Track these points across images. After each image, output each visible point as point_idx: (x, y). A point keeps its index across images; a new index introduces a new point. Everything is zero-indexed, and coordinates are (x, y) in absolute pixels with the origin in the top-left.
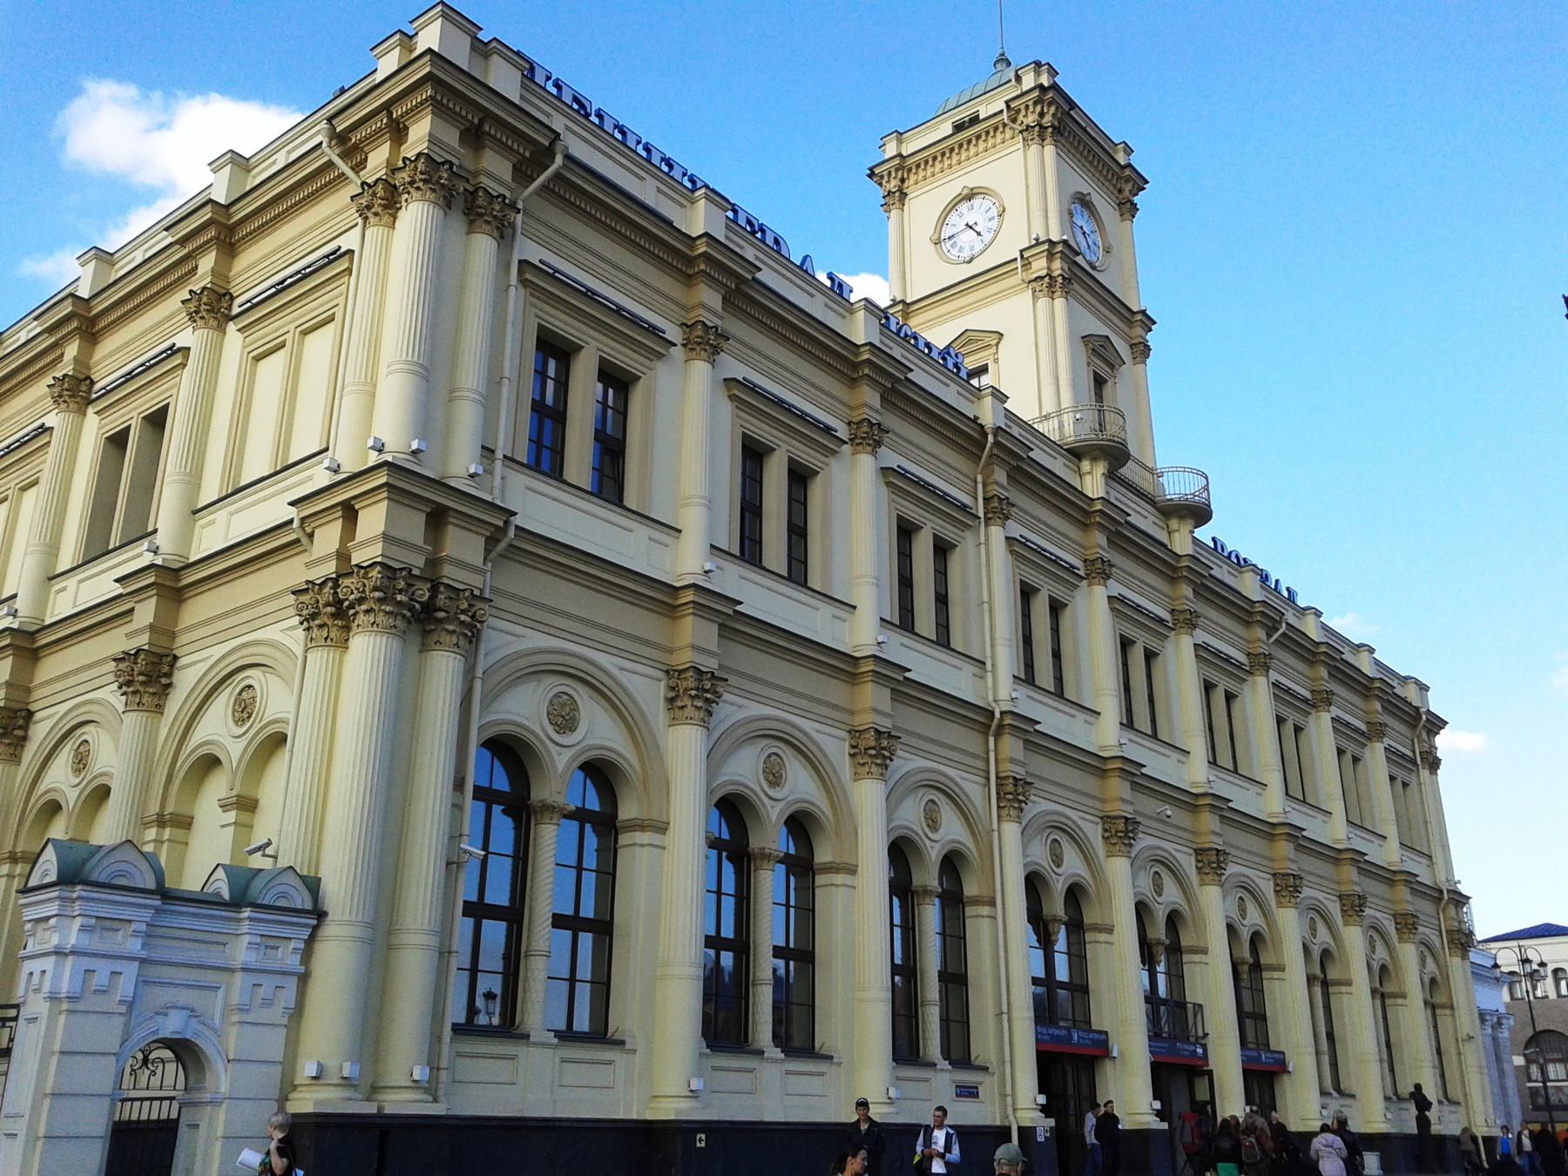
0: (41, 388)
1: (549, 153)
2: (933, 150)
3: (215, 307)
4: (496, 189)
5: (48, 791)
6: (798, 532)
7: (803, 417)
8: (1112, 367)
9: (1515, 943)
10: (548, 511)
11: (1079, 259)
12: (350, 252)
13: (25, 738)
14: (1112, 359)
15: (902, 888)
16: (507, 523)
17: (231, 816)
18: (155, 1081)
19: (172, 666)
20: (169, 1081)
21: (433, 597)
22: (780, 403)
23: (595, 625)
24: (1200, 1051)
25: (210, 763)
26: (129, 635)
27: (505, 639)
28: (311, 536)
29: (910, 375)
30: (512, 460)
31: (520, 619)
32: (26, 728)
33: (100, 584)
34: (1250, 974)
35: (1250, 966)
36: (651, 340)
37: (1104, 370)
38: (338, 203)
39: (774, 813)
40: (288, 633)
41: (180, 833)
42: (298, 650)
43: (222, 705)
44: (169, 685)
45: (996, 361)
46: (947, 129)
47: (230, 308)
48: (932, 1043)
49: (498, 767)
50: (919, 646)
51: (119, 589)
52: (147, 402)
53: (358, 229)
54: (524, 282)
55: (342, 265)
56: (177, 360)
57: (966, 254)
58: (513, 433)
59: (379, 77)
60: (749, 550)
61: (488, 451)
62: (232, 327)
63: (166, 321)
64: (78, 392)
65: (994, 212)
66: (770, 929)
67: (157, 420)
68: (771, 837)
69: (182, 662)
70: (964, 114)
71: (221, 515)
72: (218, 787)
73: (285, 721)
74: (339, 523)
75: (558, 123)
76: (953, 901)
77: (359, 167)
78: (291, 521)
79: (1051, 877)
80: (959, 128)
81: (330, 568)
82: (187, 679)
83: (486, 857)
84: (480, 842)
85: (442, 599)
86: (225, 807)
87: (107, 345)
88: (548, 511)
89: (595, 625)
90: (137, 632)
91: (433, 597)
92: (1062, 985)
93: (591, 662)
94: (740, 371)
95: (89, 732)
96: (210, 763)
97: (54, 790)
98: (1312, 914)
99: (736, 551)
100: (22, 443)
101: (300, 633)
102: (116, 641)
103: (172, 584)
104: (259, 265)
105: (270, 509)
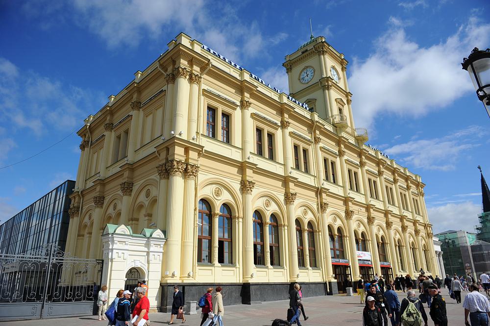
0: (102, 127)
1: (208, 64)
2: (297, 59)
3: (137, 106)
4: (196, 73)
5: (109, 214)
6: (306, 163)
7: (270, 121)
8: (343, 106)
9: (443, 235)
10: (210, 145)
11: (333, 81)
12: (165, 90)
13: (103, 203)
14: (342, 104)
15: (300, 231)
16: (202, 149)
17: (147, 218)
18: (133, 276)
19: (132, 186)
20: (136, 276)
21: (187, 167)
22: (264, 118)
23: (223, 172)
24: (370, 263)
25: (141, 206)
26: (123, 179)
27: (202, 177)
28: (159, 155)
29: (257, 89)
30: (203, 135)
31: (260, 186)
32: (103, 201)
33: (116, 169)
34: (400, 246)
35: (382, 243)
36: (233, 105)
37: (341, 107)
38: (162, 81)
39: (306, 222)
40: (155, 176)
41: (136, 222)
42: (158, 180)
43: (143, 194)
44: (132, 190)
45: (315, 106)
46: (300, 53)
47: (140, 106)
48: (204, 256)
49: (204, 206)
50: (218, 143)
51: (120, 169)
52: (124, 128)
53: (166, 85)
54: (321, 150)
55: (163, 94)
56: (130, 118)
57: (307, 82)
58: (204, 128)
59: (169, 51)
60: (260, 153)
61: (197, 133)
62: (141, 110)
63: (127, 110)
64: (110, 127)
65: (313, 71)
66: (268, 240)
67: (127, 132)
68: (218, 210)
69: (135, 184)
70: (304, 49)
71: (141, 151)
72: (143, 212)
73: (157, 196)
74: (165, 151)
75: (210, 57)
76: (312, 234)
77: (166, 71)
78: (155, 152)
79: (334, 225)
80: (303, 53)
81: (164, 162)
82: (135, 188)
83: (202, 226)
84: (201, 222)
85: (189, 167)
86: (145, 216)
87: (115, 117)
88: (210, 145)
89: (223, 172)
90: (125, 178)
91: (187, 167)
92: (337, 250)
93: (224, 181)
94: (255, 111)
95: (115, 201)
96: (141, 206)
97: (110, 214)
98: (378, 227)
99: (295, 168)
100: (99, 139)
101: (158, 177)
102: (121, 181)
103: (132, 168)
104: (147, 95)
105: (151, 149)
